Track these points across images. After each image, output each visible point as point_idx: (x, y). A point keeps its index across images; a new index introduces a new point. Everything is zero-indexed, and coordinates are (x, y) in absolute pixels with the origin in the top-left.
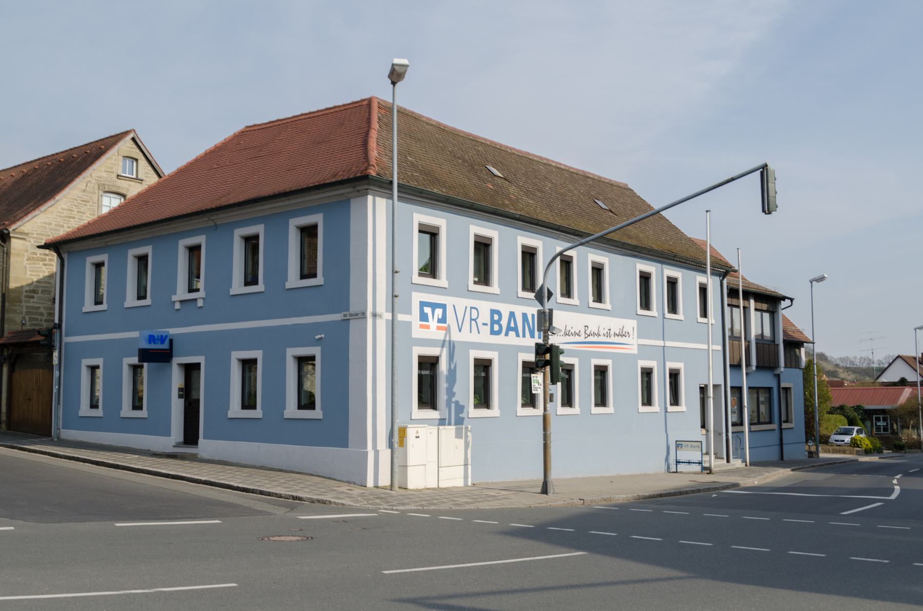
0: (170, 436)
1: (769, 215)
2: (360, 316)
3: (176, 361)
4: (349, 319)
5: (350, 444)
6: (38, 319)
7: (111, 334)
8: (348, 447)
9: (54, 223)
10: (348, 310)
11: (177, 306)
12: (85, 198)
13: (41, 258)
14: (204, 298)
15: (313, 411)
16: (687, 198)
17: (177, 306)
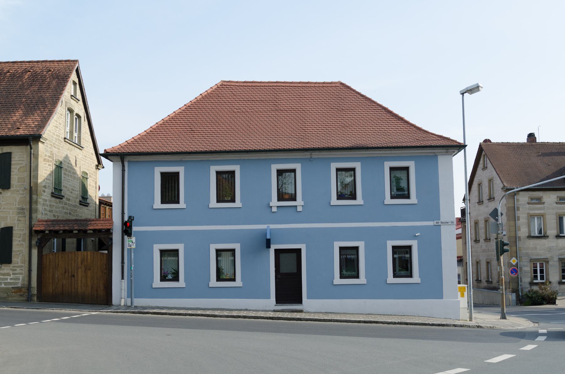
0: (270, 299)
1: (495, 199)
2: (450, 223)
3: (273, 247)
4: (440, 225)
8: (441, 297)
10: (440, 220)
11: (274, 209)
14: (302, 206)
15: (411, 279)
17: (274, 209)
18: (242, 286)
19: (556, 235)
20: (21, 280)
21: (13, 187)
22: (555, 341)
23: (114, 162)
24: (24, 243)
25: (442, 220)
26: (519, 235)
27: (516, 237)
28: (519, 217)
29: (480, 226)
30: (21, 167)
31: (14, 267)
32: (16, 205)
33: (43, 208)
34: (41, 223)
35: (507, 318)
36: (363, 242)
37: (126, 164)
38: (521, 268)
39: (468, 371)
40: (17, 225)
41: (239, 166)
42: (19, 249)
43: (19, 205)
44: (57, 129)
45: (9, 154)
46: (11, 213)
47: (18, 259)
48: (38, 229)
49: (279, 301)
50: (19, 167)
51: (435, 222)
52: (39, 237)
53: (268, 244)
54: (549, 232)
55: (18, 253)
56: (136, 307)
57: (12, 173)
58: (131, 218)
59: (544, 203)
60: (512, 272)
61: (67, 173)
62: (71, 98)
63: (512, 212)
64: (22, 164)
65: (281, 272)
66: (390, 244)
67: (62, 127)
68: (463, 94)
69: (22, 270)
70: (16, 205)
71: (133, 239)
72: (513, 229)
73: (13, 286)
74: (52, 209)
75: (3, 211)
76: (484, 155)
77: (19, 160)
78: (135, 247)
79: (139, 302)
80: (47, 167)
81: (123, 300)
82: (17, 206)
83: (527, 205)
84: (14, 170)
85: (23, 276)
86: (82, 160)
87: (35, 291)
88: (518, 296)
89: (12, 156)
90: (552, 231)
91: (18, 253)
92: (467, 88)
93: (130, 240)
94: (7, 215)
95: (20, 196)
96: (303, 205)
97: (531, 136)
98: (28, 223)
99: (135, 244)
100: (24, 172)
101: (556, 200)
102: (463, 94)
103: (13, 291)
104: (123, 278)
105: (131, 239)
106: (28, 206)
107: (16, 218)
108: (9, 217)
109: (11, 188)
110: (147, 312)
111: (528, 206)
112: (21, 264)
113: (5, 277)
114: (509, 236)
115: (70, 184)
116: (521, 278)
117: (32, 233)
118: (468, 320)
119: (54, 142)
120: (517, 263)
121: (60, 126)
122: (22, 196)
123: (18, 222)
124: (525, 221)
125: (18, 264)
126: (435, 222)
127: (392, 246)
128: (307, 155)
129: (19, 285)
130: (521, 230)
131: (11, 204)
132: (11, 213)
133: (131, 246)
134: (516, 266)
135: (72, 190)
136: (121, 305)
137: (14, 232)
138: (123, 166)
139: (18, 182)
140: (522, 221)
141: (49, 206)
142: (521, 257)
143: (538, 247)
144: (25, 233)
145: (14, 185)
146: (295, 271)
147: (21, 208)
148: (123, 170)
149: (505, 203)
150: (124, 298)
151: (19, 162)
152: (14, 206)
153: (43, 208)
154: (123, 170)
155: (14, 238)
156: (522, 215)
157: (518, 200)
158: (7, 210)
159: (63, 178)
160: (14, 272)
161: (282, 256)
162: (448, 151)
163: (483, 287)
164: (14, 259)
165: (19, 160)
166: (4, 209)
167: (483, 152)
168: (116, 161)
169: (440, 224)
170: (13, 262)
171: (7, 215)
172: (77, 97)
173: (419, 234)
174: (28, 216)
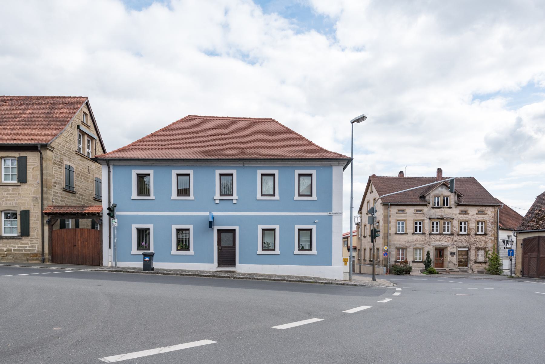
3: (216, 228)
5: (332, 265)
6: (58, 199)
7: (191, 215)
8: (332, 265)
9: (62, 144)
12: (72, 132)
13: (58, 164)
14: (237, 200)
16: (130, 161)
17: (217, 202)
18: (194, 254)
19: (413, 233)
20: (37, 248)
21: (29, 182)
22: (210, 285)
23: (103, 165)
24: (38, 222)
25: (333, 211)
26: (390, 233)
27: (388, 233)
28: (390, 222)
29: (367, 228)
30: (34, 167)
31: (31, 238)
32: (31, 195)
33: (54, 198)
34: (50, 208)
35: (376, 279)
36: (279, 226)
37: (111, 167)
38: (390, 252)
39: (321, 321)
40: (33, 209)
41: (193, 170)
42: (35, 226)
44: (67, 143)
45: (26, 157)
48: (46, 212)
49: (220, 265)
50: (33, 167)
51: (329, 213)
52: (49, 218)
53: (211, 225)
54: (408, 231)
55: (34, 229)
56: (118, 267)
57: (28, 172)
58: (115, 206)
59: (406, 213)
60: (384, 255)
61: (79, 176)
62: (82, 124)
63: (387, 218)
64: (35, 165)
65: (222, 246)
66: (297, 227)
67: (72, 143)
68: (352, 123)
69: (38, 241)
70: (31, 195)
71: (116, 220)
72: (386, 228)
73: (31, 252)
74: (64, 200)
76: (372, 184)
77: (33, 162)
78: (117, 226)
79: (122, 264)
80: (58, 169)
81: (110, 263)
82: (32, 195)
83: (396, 214)
84: (29, 169)
85: (39, 245)
86: (95, 170)
87: (47, 256)
88: (387, 269)
89: (28, 159)
90: (410, 230)
91: (34, 229)
92: (355, 118)
93: (113, 220)
94: (25, 202)
95: (34, 188)
96: (237, 199)
97: (401, 173)
99: (117, 224)
100: (37, 171)
101: (414, 212)
102: (352, 123)
103: (31, 255)
104: (110, 247)
105: (114, 220)
109: (28, 183)
110: (121, 271)
111: (396, 215)
112: (37, 237)
113: (25, 246)
114: (383, 233)
115: (83, 184)
116: (390, 258)
117: (44, 214)
118: (349, 280)
119: (64, 152)
120: (388, 249)
121: (70, 142)
122: (36, 188)
123: (33, 207)
124: (394, 223)
125: (34, 236)
126: (329, 213)
127: (299, 229)
128: (240, 163)
129: (36, 252)
130: (391, 229)
131: (27, 194)
132: (28, 200)
133: (114, 225)
134: (387, 251)
135: (85, 189)
137: (31, 214)
138: (109, 168)
139: (33, 178)
140: (393, 224)
141: (60, 197)
142: (391, 246)
143: (401, 240)
144: (39, 215)
146: (232, 245)
147: (35, 197)
148: (109, 171)
149: (382, 212)
150: (111, 262)
151: (32, 164)
152: (30, 195)
153: (54, 198)
154: (109, 171)
155: (30, 218)
156: (393, 220)
157: (390, 211)
159: (75, 180)
160: (31, 242)
161: (223, 235)
162: (339, 163)
163: (367, 264)
164: (31, 233)
165: (33, 162)
166: (22, 197)
167: (371, 182)
169: (332, 214)
170: (30, 235)
171: (25, 202)
172: (89, 125)
173: (317, 221)
174: (40, 203)
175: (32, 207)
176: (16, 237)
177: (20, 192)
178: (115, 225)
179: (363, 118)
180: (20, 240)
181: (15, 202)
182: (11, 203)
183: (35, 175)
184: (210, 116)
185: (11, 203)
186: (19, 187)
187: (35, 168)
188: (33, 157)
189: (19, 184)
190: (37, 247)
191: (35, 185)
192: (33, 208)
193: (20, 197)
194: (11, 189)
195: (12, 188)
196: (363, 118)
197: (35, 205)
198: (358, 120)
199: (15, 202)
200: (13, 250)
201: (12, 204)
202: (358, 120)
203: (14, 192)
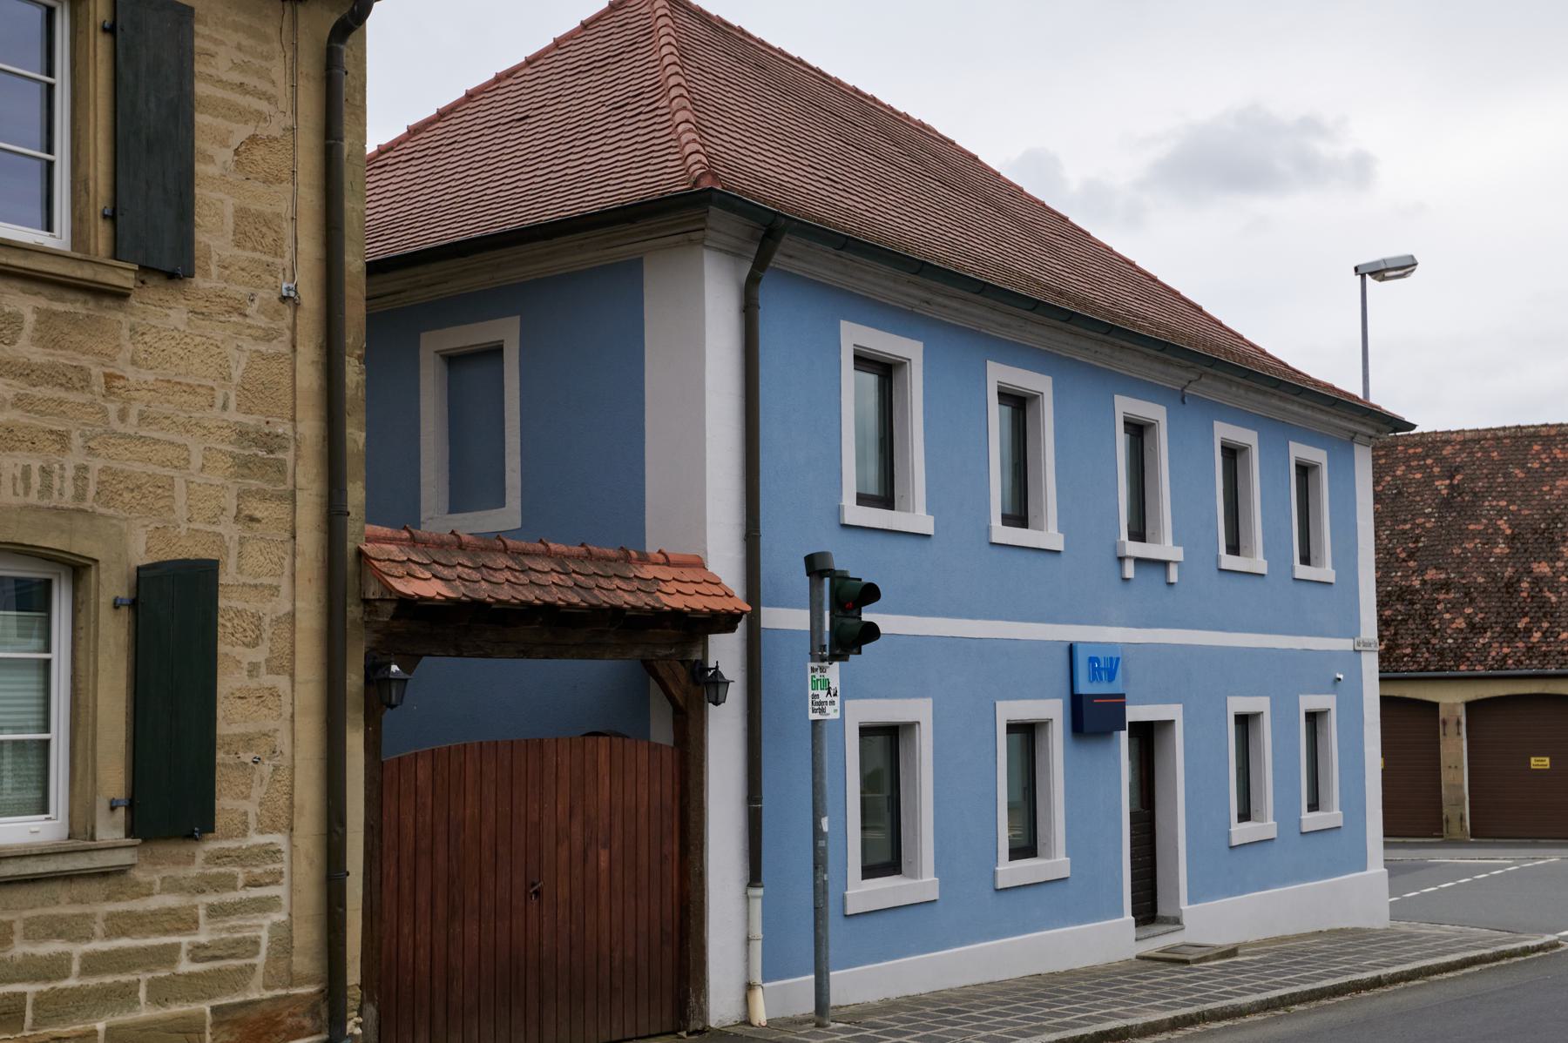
21: (207, 274)
32: (225, 407)
42: (251, 728)
43: (249, 411)
46: (197, 461)
47: (247, 797)
55: (247, 757)
64: (260, 116)
70: (225, 407)
75: (142, 439)
82: (233, 416)
85: (280, 917)
91: (247, 757)
93: (818, 675)
95: (248, 345)
98: (310, 541)
106: (310, 427)
107: (230, 502)
108: (180, 485)
109: (198, 280)
127: (1236, 716)
131: (192, 390)
132: (197, 461)
133: (822, 711)
136: (756, 1022)
145: (215, 258)
158: (172, 436)
166: (143, 418)
168: (721, 250)
175: (230, 531)
176: (42, 854)
177: (122, 366)
178: (829, 709)
179: (1404, 267)
180: (112, 880)
181: (73, 459)
182: (26, 471)
183: (259, 215)
184: (815, 66)
185: (26, 471)
186: (107, 302)
187: (259, 153)
188: (246, 42)
189: (122, 277)
190: (264, 943)
191: (261, 311)
192: (242, 541)
193: (123, 415)
194: (30, 318)
195: (37, 310)
196: (1404, 267)
197: (259, 510)
198: (1380, 272)
199: (73, 459)
200: (37, 1004)
201: (36, 480)
202: (1380, 272)
203: (62, 357)
